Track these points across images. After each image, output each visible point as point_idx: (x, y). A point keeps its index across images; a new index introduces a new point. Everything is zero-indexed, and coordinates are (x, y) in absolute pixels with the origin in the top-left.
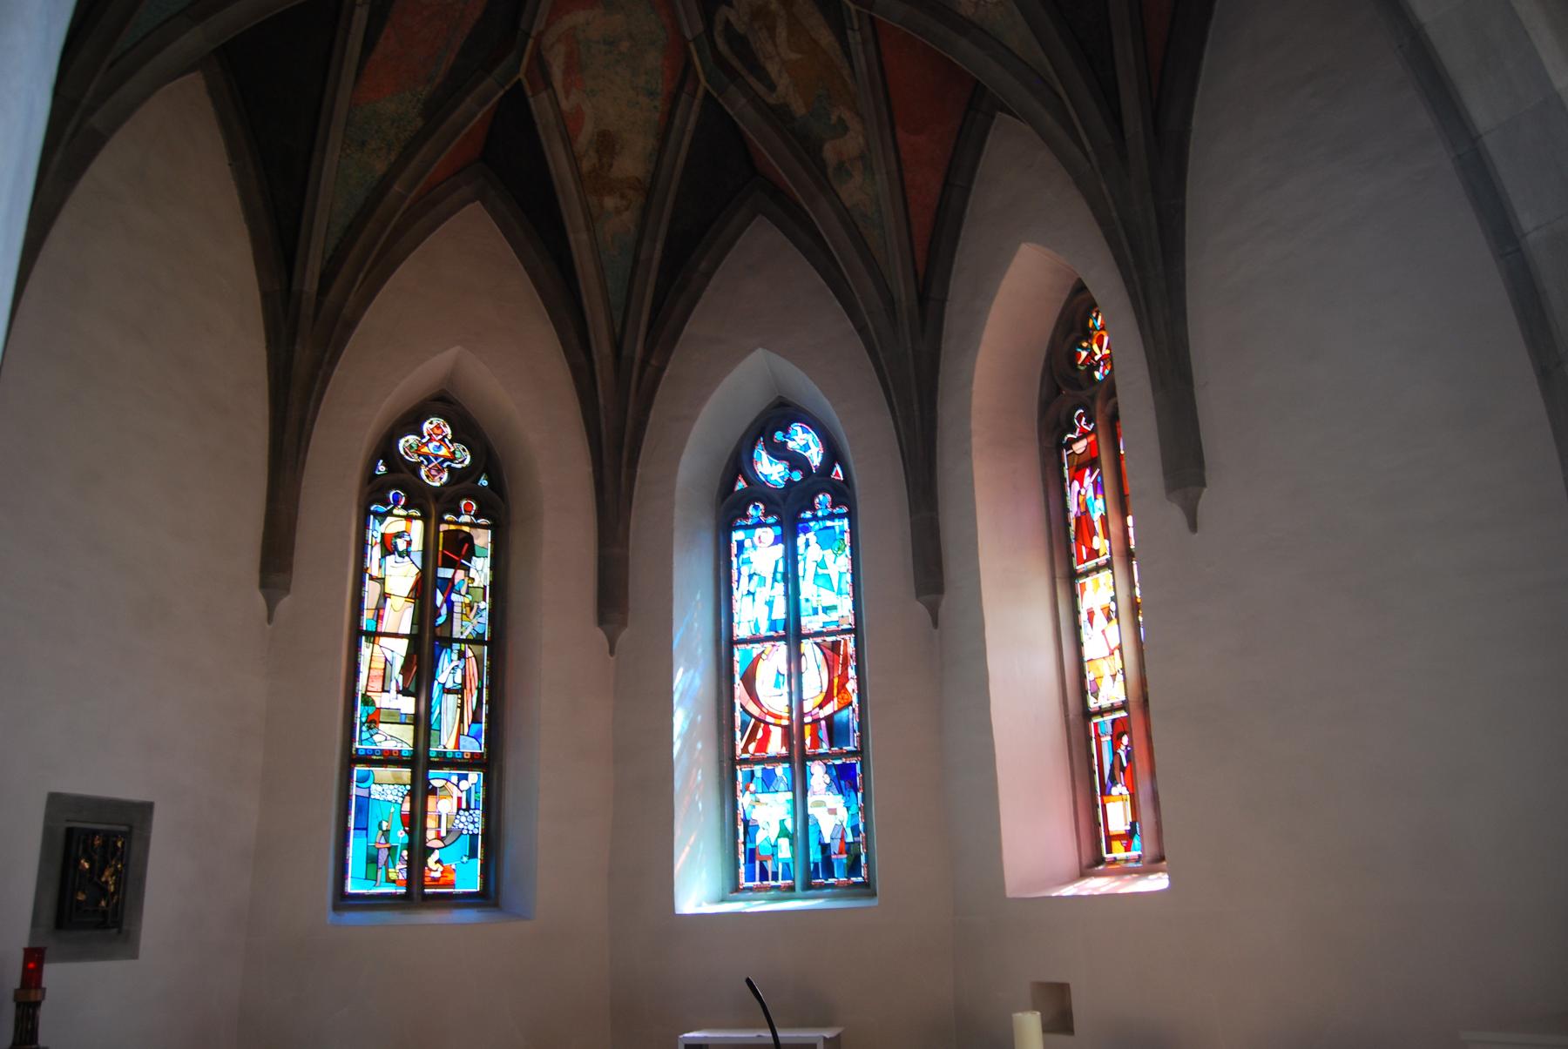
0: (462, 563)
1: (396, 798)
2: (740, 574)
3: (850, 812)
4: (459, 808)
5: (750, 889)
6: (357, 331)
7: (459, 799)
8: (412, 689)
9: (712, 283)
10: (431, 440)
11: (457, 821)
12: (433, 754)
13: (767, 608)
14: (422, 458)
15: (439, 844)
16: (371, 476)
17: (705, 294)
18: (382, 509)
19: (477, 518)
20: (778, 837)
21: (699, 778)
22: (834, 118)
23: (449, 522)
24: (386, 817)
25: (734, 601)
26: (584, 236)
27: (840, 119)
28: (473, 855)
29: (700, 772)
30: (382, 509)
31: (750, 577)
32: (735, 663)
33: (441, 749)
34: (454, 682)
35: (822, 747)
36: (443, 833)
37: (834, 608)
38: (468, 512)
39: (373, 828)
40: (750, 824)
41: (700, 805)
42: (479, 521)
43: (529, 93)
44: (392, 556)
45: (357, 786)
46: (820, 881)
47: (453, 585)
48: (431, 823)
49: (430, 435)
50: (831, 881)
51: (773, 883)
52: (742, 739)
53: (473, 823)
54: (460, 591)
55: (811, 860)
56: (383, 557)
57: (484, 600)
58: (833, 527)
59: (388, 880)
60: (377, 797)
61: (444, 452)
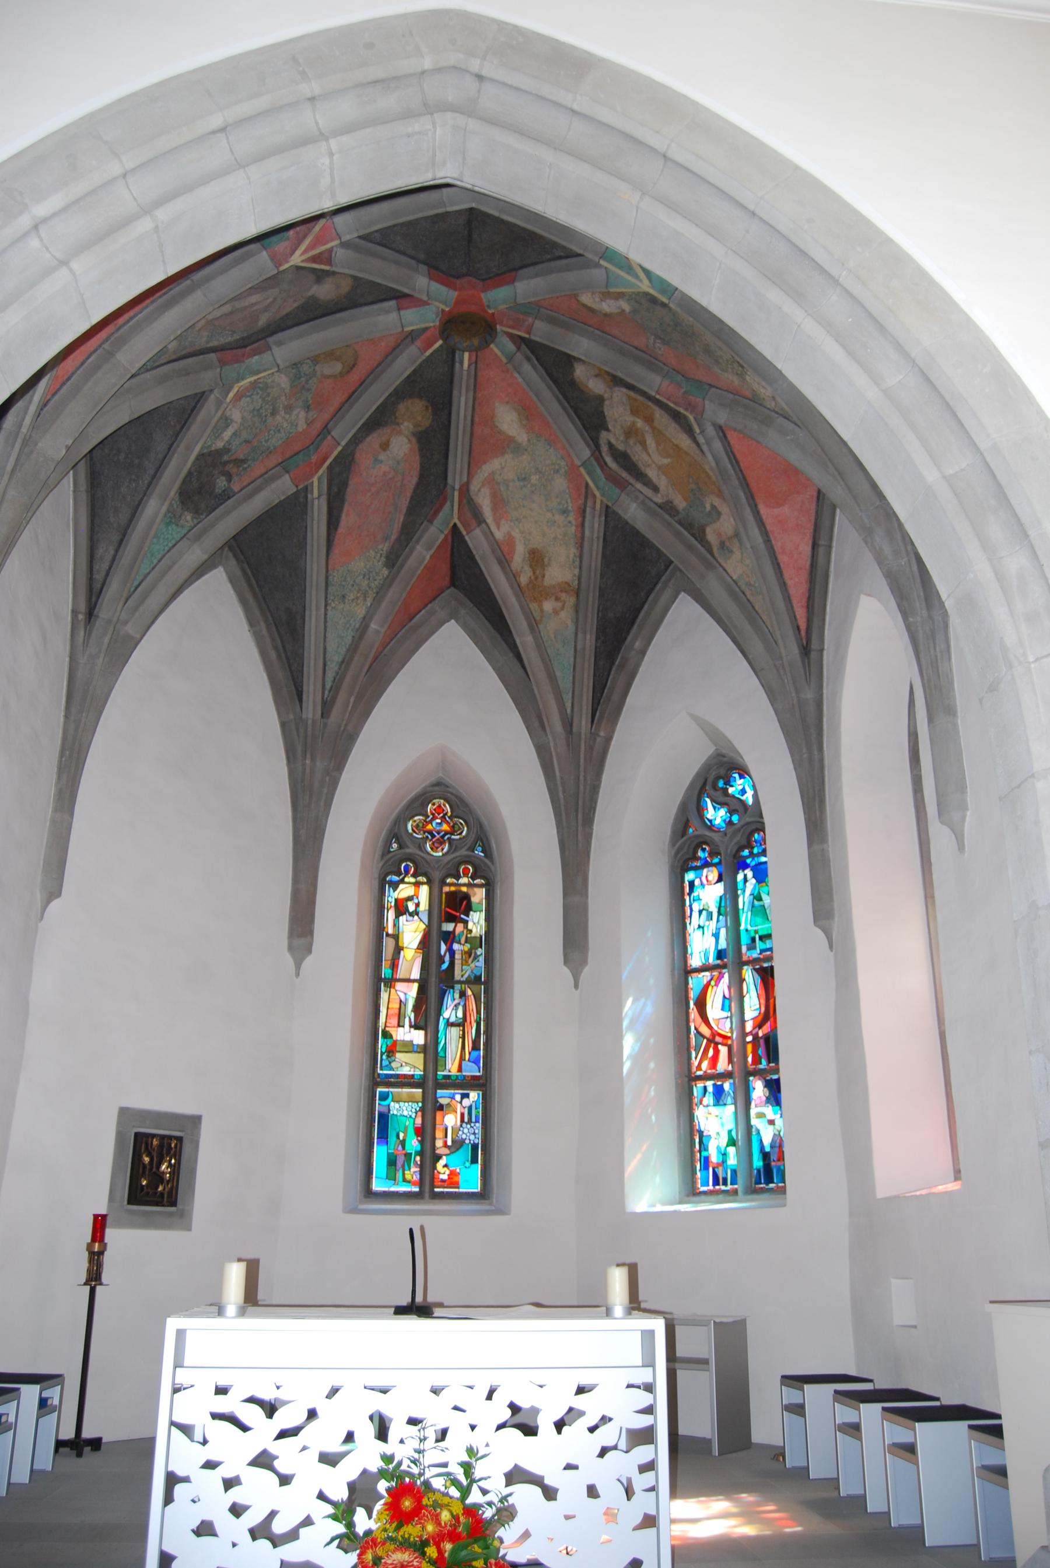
0: (462, 919)
1: (410, 1113)
2: (691, 910)
4: (462, 1120)
5: (704, 1193)
7: (462, 1115)
8: (422, 1024)
10: (434, 818)
11: (460, 1133)
12: (440, 1077)
13: (713, 939)
14: (426, 834)
15: (446, 1151)
16: (386, 850)
18: (395, 878)
19: (473, 879)
20: (727, 1146)
21: (652, 1093)
22: (708, 507)
23: (450, 885)
25: (687, 935)
26: (529, 639)
27: (713, 507)
28: (474, 1160)
30: (395, 878)
31: (700, 912)
32: (690, 990)
34: (456, 1017)
35: (761, 1063)
36: (449, 1143)
38: (466, 874)
39: (392, 1139)
40: (705, 1134)
41: (653, 1118)
42: (475, 882)
43: (464, 533)
44: (405, 916)
45: (379, 1104)
46: (762, 1186)
47: (454, 936)
48: (439, 1134)
49: (433, 814)
50: (771, 1185)
51: (723, 1188)
52: (696, 1058)
53: (472, 1134)
54: (460, 941)
55: (755, 1167)
56: (397, 916)
57: (481, 947)
59: (405, 1180)
60: (395, 1112)
61: (445, 827)
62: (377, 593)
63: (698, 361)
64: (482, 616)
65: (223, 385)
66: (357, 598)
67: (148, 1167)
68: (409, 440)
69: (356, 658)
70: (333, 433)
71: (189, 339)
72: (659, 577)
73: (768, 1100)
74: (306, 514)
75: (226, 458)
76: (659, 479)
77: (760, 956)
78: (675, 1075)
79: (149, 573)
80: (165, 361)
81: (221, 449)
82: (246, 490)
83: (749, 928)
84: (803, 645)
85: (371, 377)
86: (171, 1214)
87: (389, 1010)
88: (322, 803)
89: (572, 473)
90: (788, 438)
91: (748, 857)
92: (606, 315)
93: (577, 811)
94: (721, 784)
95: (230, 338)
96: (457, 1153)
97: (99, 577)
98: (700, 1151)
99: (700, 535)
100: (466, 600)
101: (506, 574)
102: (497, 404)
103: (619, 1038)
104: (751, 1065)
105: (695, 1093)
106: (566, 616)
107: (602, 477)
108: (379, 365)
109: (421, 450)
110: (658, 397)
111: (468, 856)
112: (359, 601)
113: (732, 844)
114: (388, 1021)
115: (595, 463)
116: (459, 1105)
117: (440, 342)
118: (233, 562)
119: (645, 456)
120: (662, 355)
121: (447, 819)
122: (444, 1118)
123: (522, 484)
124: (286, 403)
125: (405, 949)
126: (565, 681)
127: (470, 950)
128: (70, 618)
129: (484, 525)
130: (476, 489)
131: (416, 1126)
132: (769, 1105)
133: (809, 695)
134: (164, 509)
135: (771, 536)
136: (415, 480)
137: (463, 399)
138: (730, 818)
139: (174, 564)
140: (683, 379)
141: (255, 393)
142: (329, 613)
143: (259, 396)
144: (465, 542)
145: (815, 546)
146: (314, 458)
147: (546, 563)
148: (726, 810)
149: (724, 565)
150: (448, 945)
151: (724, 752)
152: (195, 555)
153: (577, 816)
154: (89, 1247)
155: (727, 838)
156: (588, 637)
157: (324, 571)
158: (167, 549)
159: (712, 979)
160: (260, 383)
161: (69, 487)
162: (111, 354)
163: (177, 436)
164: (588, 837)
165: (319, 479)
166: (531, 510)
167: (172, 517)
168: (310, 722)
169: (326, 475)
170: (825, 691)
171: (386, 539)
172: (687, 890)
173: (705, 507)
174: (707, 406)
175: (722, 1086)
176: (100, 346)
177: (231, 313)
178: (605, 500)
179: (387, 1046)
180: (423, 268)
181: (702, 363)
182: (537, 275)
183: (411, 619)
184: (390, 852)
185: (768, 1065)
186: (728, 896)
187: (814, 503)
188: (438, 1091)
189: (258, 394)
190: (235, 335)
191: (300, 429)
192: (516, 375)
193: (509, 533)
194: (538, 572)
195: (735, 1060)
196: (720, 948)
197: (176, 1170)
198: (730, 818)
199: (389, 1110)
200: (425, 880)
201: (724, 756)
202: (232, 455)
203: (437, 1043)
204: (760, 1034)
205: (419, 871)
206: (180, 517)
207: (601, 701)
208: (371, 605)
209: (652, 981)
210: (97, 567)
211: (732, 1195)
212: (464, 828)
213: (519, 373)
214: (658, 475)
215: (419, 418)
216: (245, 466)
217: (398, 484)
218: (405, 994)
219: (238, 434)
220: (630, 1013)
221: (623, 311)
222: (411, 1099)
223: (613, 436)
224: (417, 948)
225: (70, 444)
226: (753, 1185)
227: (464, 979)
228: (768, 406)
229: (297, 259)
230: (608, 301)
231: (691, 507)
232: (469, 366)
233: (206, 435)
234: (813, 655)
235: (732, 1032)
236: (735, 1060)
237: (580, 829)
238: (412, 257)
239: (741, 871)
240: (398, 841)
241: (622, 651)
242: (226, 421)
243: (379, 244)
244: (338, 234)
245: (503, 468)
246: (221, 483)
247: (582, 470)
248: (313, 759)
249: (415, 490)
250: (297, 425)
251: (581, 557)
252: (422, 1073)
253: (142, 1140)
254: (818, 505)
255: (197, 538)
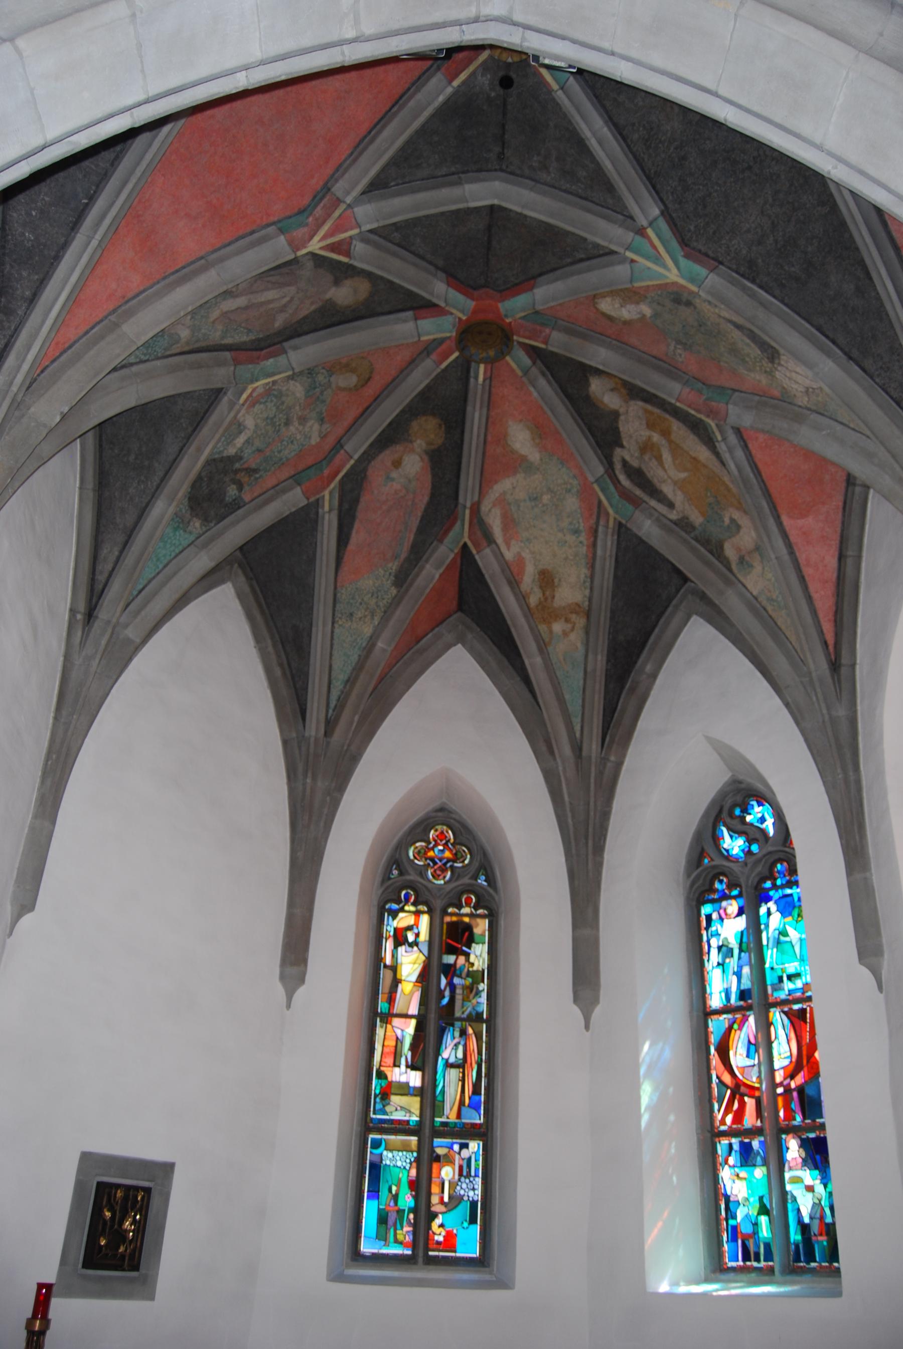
1: (404, 1164)
3: (827, 1190)
4: (461, 1174)
6: (362, 762)
7: (461, 1168)
9: (659, 681)
10: (436, 845)
11: (458, 1188)
14: (428, 861)
15: (441, 1208)
16: (386, 877)
17: (652, 693)
18: (395, 906)
19: (476, 910)
21: (673, 1151)
22: (727, 521)
23: (452, 914)
24: (395, 1182)
25: (706, 973)
26: (538, 660)
27: (733, 520)
28: (473, 1221)
29: (673, 1144)
30: (395, 906)
31: (720, 948)
33: (444, 1119)
35: (795, 1119)
36: (446, 1199)
37: (798, 975)
38: (468, 904)
40: (731, 1199)
41: (675, 1179)
43: (474, 552)
44: (403, 947)
45: (371, 1153)
46: (802, 1264)
48: (435, 1189)
50: (813, 1265)
51: (755, 1264)
54: (461, 974)
55: (792, 1241)
58: (791, 895)
59: (396, 1241)
60: (388, 1162)
61: (447, 854)
62: (385, 612)
63: (722, 364)
64: (489, 641)
65: (237, 384)
66: (365, 616)
67: (109, 1223)
68: (421, 458)
69: (362, 677)
70: (346, 448)
71: (203, 331)
72: (670, 600)
73: (805, 1162)
74: (317, 531)
75: (237, 466)
76: (675, 495)
77: (788, 997)
78: (697, 1130)
79: (154, 578)
80: (178, 351)
81: (233, 457)
82: (257, 500)
83: (775, 966)
84: (831, 660)
85: (386, 392)
86: (132, 1280)
87: (385, 1048)
88: (322, 824)
89: (585, 492)
90: (824, 432)
91: (770, 889)
92: (626, 323)
93: (586, 838)
94: (737, 812)
95: (245, 337)
96: (454, 1211)
97: (101, 578)
98: (727, 1220)
99: (717, 550)
100: (474, 626)
101: (515, 595)
102: (510, 423)
103: (637, 1087)
104: (784, 1121)
105: (719, 1152)
106: (576, 638)
107: (616, 494)
108: (394, 380)
109: (432, 469)
110: (678, 404)
111: (470, 885)
112: (367, 620)
113: (753, 875)
114: (383, 1060)
115: (609, 481)
116: (457, 1157)
117: (456, 354)
118: (242, 579)
119: (660, 472)
120: (682, 362)
121: (450, 846)
122: (440, 1170)
123: (533, 504)
124: (300, 413)
125: (403, 982)
126: (574, 705)
127: (472, 984)
128: (67, 617)
129: (494, 546)
130: (487, 509)
131: (410, 1178)
132: (806, 1168)
133: (841, 712)
134: (171, 510)
135: (795, 548)
136: (426, 499)
137: (477, 415)
138: (749, 847)
139: (180, 569)
140: (704, 387)
141: (269, 400)
142: (337, 631)
143: (273, 404)
144: (475, 561)
145: (841, 557)
146: (326, 472)
147: (556, 584)
148: (744, 838)
149: (744, 581)
150: (449, 978)
151: (741, 777)
152: (202, 562)
153: (587, 843)
154: (30, 1323)
155: (746, 870)
156: (599, 657)
157: (332, 587)
158: (173, 554)
159: (734, 1022)
160: (274, 390)
161: (75, 481)
162: (117, 325)
163: (188, 439)
164: (599, 865)
165: (331, 493)
166: (542, 530)
167: (179, 522)
168: (312, 740)
169: (337, 490)
170: (859, 708)
171: (395, 557)
172: (704, 924)
173: (723, 521)
174: (730, 411)
175: (750, 1143)
176: (106, 317)
177: (246, 308)
178: (617, 516)
179: (381, 1087)
180: (442, 275)
181: (726, 365)
182: (556, 280)
183: (418, 642)
184: (389, 879)
185: (803, 1121)
186: (751, 931)
187: (840, 515)
188: (435, 1140)
189: (272, 401)
190: (250, 334)
191: (313, 442)
192: (532, 389)
193: (519, 553)
194: (547, 593)
195: (766, 1114)
196: (742, 987)
197: (141, 1228)
198: (749, 847)
199: (381, 1160)
200: (426, 909)
201: (740, 782)
202: (244, 463)
203: (435, 1086)
204: (793, 1085)
205: (420, 899)
206: (189, 522)
207: (612, 725)
208: (379, 624)
209: (669, 1023)
210: (100, 568)
211: (767, 1275)
212: (466, 855)
213: (534, 386)
214: (674, 491)
215: (432, 436)
216: (257, 476)
217: (410, 503)
218: (402, 1030)
219: (251, 441)
220: (647, 1059)
221: (644, 316)
222: (405, 1148)
223: (627, 453)
224: (417, 982)
225: (65, 411)
226: (792, 1263)
227: (465, 1016)
228: (800, 404)
229: (315, 245)
230: (628, 306)
231: (708, 522)
232: (484, 380)
233: (217, 436)
234: (844, 671)
235: (760, 1083)
236: (766, 1114)
237: (590, 857)
238: (430, 263)
239: (763, 904)
240: (399, 868)
241: (633, 674)
242: (240, 428)
243: (399, 245)
244: (357, 223)
245: (514, 488)
246: (232, 491)
247: (596, 486)
248: (314, 778)
249: (426, 510)
250: (310, 438)
251: (592, 577)
252: (418, 1119)
253: (104, 1190)
254: (844, 516)
255: (205, 545)
